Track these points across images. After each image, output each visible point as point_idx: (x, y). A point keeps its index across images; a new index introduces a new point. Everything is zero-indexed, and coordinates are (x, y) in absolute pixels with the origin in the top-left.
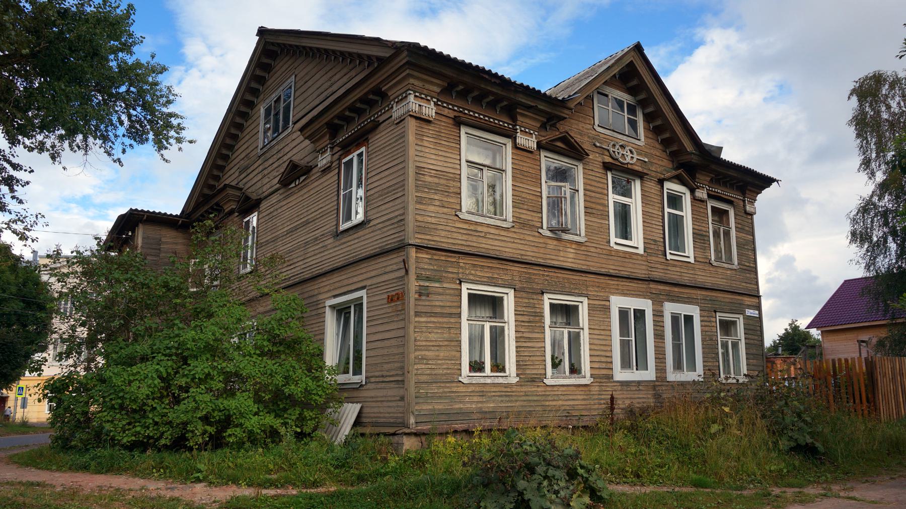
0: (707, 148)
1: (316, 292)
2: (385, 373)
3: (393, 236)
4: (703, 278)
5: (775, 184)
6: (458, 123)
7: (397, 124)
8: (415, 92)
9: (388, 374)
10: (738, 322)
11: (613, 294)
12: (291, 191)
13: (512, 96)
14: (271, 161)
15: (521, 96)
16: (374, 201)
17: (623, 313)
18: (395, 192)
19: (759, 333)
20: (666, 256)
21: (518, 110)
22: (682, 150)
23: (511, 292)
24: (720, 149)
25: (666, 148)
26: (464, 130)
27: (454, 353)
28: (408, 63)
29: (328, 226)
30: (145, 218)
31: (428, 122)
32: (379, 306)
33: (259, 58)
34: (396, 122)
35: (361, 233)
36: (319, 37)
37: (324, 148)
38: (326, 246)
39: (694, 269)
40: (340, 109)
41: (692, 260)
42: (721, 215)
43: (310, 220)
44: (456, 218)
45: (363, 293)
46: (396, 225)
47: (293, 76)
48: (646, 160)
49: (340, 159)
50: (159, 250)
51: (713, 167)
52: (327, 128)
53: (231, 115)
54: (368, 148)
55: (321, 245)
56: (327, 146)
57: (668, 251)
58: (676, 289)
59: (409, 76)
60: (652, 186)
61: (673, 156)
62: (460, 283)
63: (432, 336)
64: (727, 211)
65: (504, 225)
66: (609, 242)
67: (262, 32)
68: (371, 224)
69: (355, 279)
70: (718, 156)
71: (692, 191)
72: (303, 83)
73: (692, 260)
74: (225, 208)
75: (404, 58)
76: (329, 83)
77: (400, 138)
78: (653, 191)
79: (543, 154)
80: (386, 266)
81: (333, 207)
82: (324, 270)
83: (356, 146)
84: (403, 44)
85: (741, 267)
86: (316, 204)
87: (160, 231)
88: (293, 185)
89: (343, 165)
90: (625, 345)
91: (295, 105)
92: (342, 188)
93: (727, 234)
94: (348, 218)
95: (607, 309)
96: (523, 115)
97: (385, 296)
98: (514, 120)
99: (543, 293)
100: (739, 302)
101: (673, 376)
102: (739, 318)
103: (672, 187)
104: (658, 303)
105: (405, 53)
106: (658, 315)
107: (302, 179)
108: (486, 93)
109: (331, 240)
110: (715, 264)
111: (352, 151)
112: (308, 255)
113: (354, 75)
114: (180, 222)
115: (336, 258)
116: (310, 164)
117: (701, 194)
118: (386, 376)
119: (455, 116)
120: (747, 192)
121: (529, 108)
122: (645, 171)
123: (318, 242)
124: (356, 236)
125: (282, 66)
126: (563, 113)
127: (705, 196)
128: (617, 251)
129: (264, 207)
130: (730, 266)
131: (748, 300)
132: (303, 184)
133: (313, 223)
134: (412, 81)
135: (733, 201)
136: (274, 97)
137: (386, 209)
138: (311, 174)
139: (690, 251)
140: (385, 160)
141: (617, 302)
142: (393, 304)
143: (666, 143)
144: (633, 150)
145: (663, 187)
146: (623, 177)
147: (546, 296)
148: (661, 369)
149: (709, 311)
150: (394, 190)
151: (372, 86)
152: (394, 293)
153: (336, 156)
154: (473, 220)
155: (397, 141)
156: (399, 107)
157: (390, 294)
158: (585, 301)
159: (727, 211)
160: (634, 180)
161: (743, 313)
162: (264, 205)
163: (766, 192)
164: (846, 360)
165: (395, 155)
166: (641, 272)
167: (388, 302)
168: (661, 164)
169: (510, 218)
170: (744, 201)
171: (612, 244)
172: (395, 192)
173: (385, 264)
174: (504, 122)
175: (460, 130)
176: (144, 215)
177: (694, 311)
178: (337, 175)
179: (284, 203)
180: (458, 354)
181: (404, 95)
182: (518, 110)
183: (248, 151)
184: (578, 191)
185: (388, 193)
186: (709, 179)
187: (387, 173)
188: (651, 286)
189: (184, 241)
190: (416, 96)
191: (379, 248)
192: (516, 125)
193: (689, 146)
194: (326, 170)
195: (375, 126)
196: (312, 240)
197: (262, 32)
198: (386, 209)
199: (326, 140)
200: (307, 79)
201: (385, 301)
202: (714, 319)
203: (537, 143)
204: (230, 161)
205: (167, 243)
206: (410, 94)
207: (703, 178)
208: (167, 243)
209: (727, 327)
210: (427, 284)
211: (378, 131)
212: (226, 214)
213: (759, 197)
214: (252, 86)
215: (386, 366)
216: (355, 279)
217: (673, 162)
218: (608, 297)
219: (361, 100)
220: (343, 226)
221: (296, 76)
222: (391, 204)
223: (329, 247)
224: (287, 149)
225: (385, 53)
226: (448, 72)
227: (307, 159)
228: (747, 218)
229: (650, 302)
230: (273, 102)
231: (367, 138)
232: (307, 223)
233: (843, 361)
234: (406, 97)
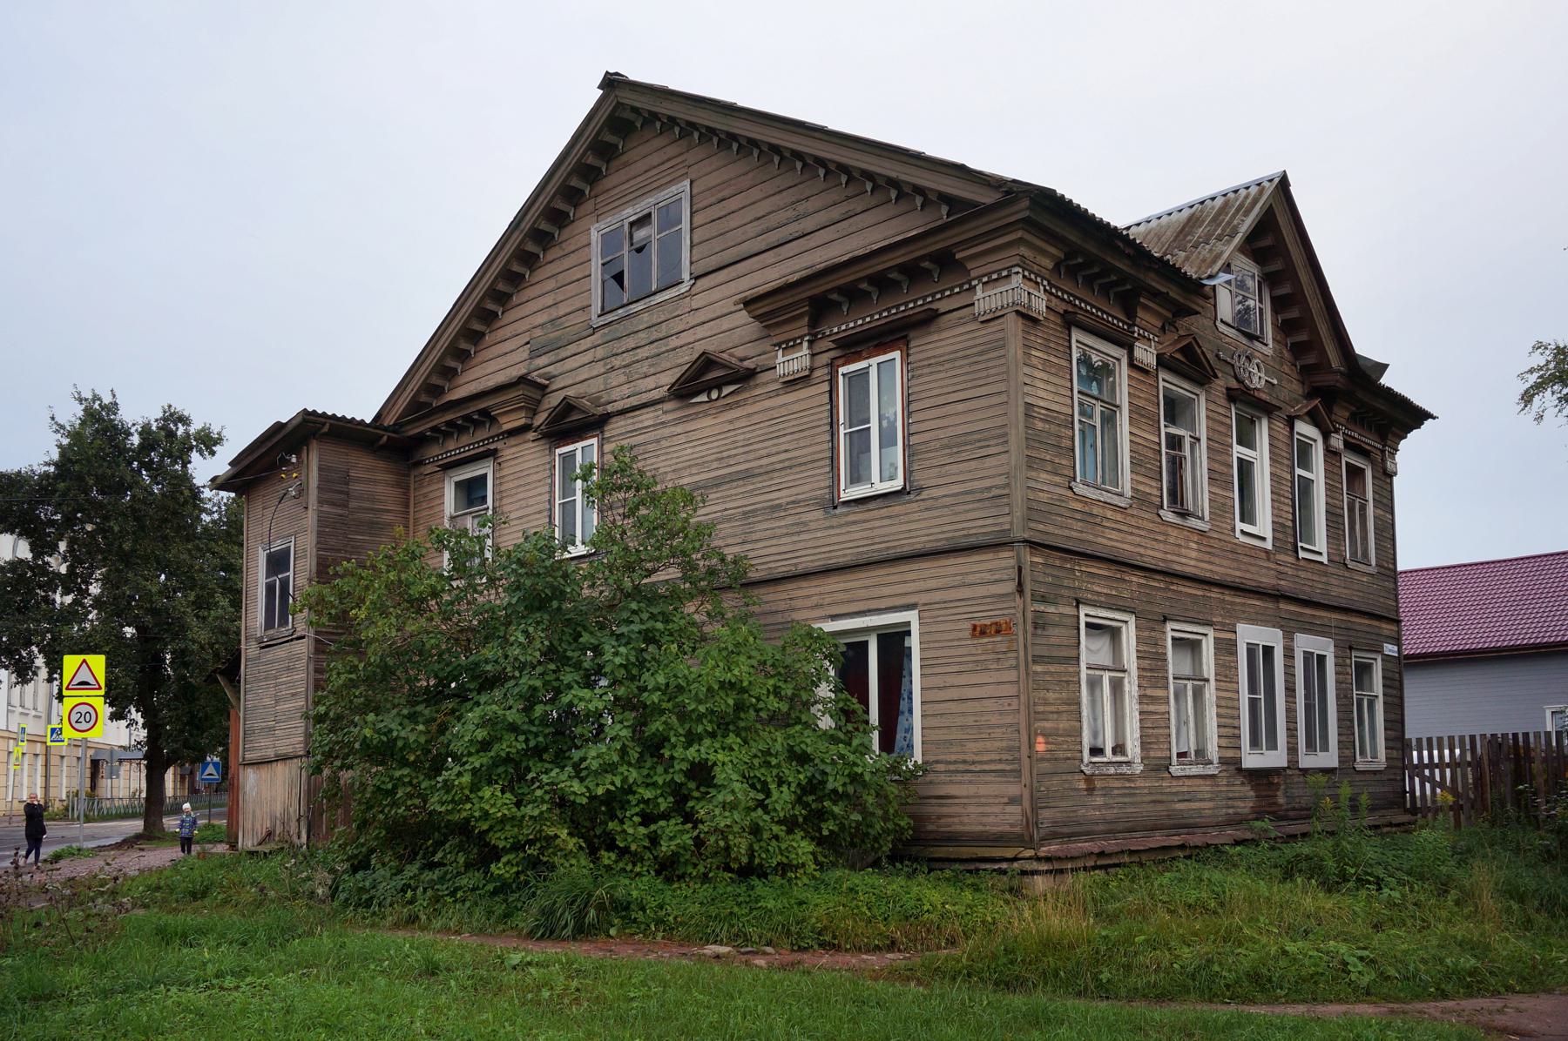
0: (1361, 362)
1: (782, 606)
2: (969, 757)
3: (981, 523)
4: (1339, 591)
5: (1428, 423)
6: (1069, 321)
7: (982, 322)
8: (1024, 269)
9: (977, 758)
10: (1124, 629)
11: (1239, 619)
12: (692, 411)
13: (1141, 276)
14: (630, 342)
15: (1152, 275)
16: (926, 456)
17: (1251, 649)
18: (983, 444)
19: (1397, 683)
20: (1297, 553)
21: (1142, 300)
22: (1323, 365)
23: (1132, 620)
24: (1383, 368)
25: (1296, 359)
26: (1076, 335)
27: (1073, 723)
28: (1026, 222)
29: (806, 488)
30: (326, 429)
31: (1035, 321)
32: (952, 640)
33: (598, 134)
34: (981, 319)
35: (897, 509)
36: (800, 130)
37: (794, 340)
38: (804, 524)
39: (1325, 574)
40: (853, 277)
41: (1324, 559)
42: (1355, 474)
43: (757, 471)
44: (1069, 494)
45: (912, 617)
46: (987, 504)
47: (687, 183)
48: (1275, 382)
49: (833, 366)
50: (347, 494)
51: (1360, 394)
52: (810, 306)
53: (517, 237)
54: (908, 355)
55: (789, 520)
56: (802, 337)
57: (1300, 544)
58: (1308, 611)
59: (1021, 241)
60: (1280, 426)
61: (1306, 372)
62: (1077, 607)
63: (1051, 696)
64: (1363, 470)
65: (1116, 500)
66: (1234, 530)
67: (612, 83)
68: (924, 495)
69: (887, 591)
70: (1374, 377)
71: (1326, 436)
72: (713, 200)
73: (1324, 559)
74: (502, 420)
75: (1022, 209)
76: (790, 214)
77: (995, 349)
78: (1281, 437)
79: (1162, 375)
80: (967, 574)
81: (820, 452)
82: (800, 567)
83: (876, 346)
84: (1025, 188)
85: (1382, 570)
86: (771, 443)
87: (347, 454)
88: (703, 398)
89: (841, 378)
90: (1253, 704)
91: (696, 241)
92: (841, 421)
93: (1363, 508)
94: (856, 477)
95: (1234, 643)
96: (1146, 308)
97: (968, 625)
98: (1131, 314)
99: (1165, 619)
100: (1377, 631)
101: (1306, 761)
102: (1206, 635)
103: (1304, 429)
104: (1289, 636)
105: (1025, 203)
106: (1289, 654)
107: (726, 390)
108: (1108, 270)
109: (819, 514)
110: (1351, 565)
111: (864, 354)
112: (754, 537)
113: (859, 210)
114: (385, 438)
115: (836, 547)
116: (747, 364)
117: (1337, 442)
118: (974, 763)
119: (1066, 311)
120: (1390, 437)
121: (1155, 295)
122: (1274, 402)
123: (783, 514)
124: (884, 512)
125: (646, 154)
126: (1198, 305)
127: (1342, 446)
128: (1244, 546)
129: (617, 431)
130: (1362, 568)
131: (1387, 628)
132: (729, 400)
133: (765, 477)
134: (1023, 250)
135: (1370, 452)
136: (631, 213)
137: (961, 472)
138: (752, 383)
139: (1321, 542)
140: (947, 386)
141: (1249, 634)
142: (985, 640)
143: (1297, 350)
144: (1262, 365)
145: (1292, 428)
146: (1249, 412)
147: (1170, 626)
148: (1292, 750)
149: (1345, 648)
150: (979, 441)
151: (938, 247)
152: (988, 622)
153: (825, 359)
154: (1088, 495)
155: (981, 353)
156: (987, 294)
157: (977, 623)
158: (1211, 633)
159: (1363, 470)
160: (1259, 418)
161: (1380, 651)
162: (616, 427)
163: (1414, 435)
164: (1526, 735)
165: (980, 378)
166: (1267, 580)
167: (974, 636)
168: (1290, 390)
169: (1128, 493)
170: (1383, 452)
171: (1238, 534)
172: (983, 444)
173: (963, 569)
174: (1114, 317)
175: (1070, 336)
176: (324, 424)
177: (1324, 646)
178: (827, 395)
179: (679, 429)
180: (1077, 724)
181: (1005, 273)
182: (1142, 300)
183: (554, 313)
184: (1199, 440)
185: (966, 444)
186: (1347, 414)
187: (960, 407)
188: (1282, 606)
189: (387, 477)
190: (1024, 277)
191: (947, 539)
192: (1135, 325)
193: (1335, 361)
194: (793, 383)
195: (929, 319)
196: (764, 508)
197: (612, 83)
198: (961, 472)
199: (801, 327)
200: (726, 193)
201: (967, 634)
202: (1348, 661)
203: (1158, 356)
204: (498, 325)
205: (359, 480)
206: (1018, 273)
207: (1341, 414)
208: (359, 480)
209: (1364, 670)
210: (1042, 608)
211: (933, 328)
212: (503, 433)
213: (1403, 444)
214: (572, 184)
215: (971, 746)
216: (887, 591)
217: (1303, 383)
218: (1234, 626)
219: (902, 268)
220: (849, 493)
221: (692, 182)
222: (973, 464)
223: (813, 526)
224: (677, 325)
225: (987, 197)
226: (1073, 236)
227: (740, 352)
228: (1386, 476)
229: (1279, 633)
230: (626, 223)
231: (905, 337)
232: (747, 476)
233: (1520, 736)
234: (1008, 276)
